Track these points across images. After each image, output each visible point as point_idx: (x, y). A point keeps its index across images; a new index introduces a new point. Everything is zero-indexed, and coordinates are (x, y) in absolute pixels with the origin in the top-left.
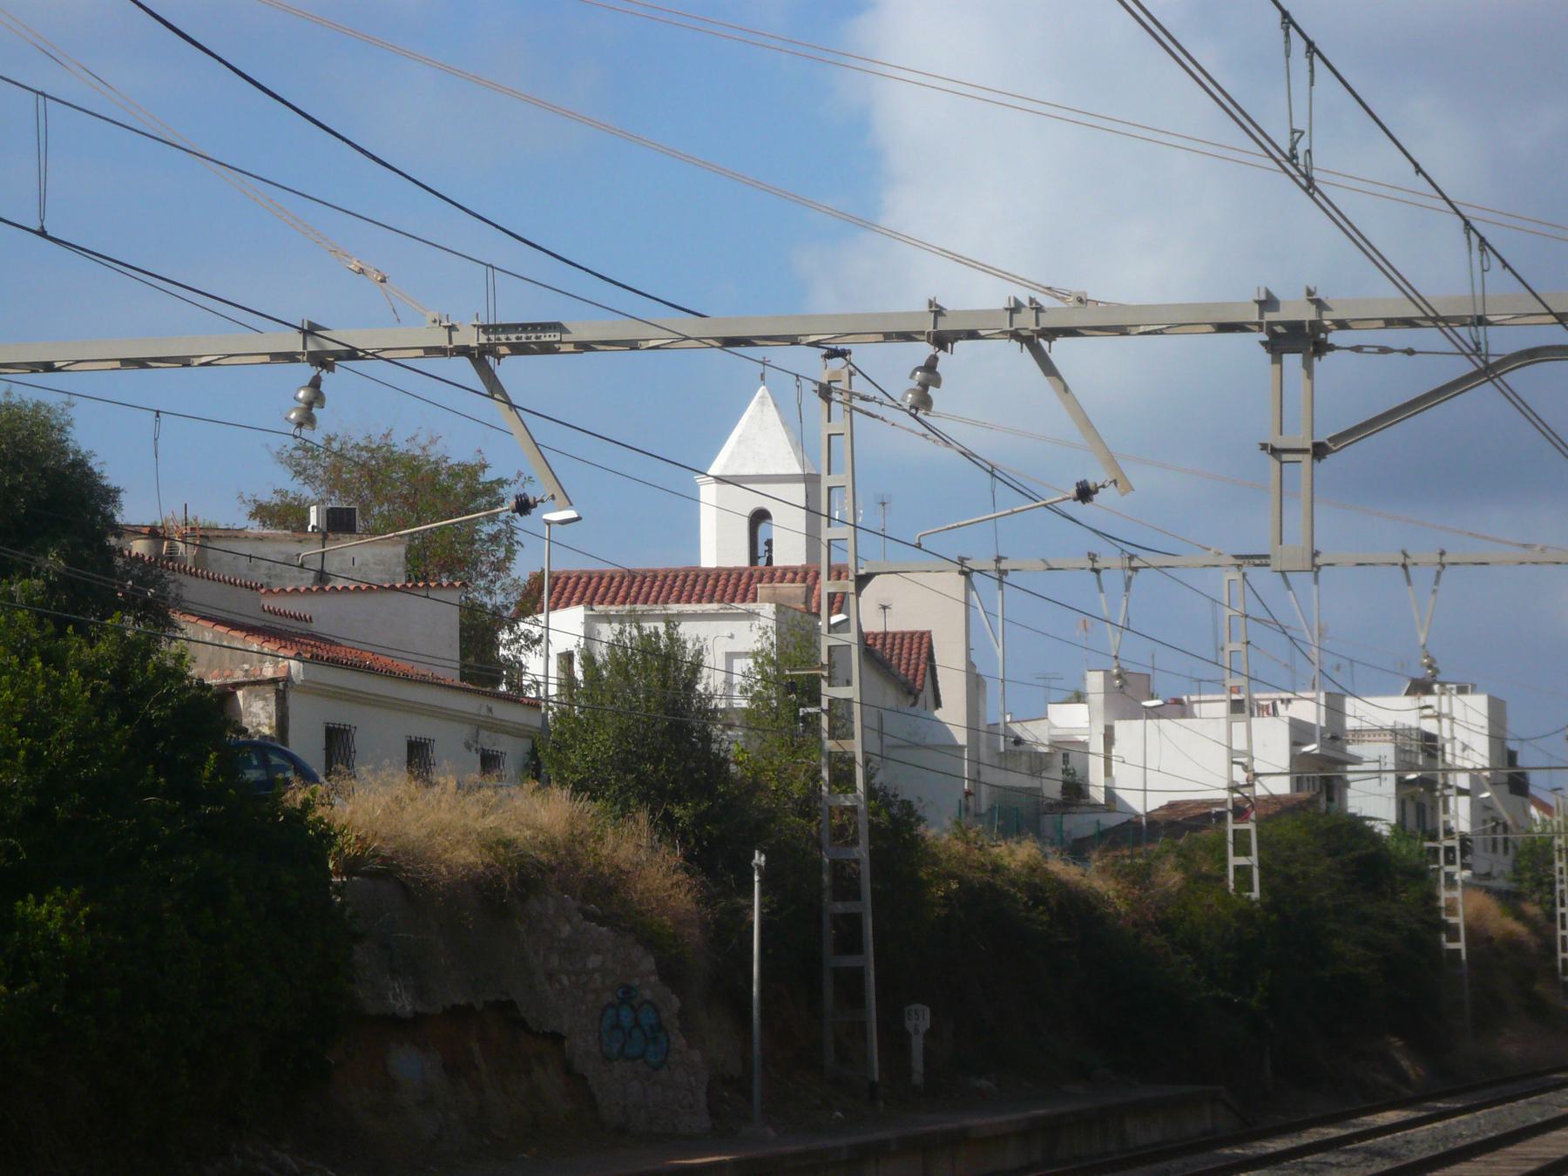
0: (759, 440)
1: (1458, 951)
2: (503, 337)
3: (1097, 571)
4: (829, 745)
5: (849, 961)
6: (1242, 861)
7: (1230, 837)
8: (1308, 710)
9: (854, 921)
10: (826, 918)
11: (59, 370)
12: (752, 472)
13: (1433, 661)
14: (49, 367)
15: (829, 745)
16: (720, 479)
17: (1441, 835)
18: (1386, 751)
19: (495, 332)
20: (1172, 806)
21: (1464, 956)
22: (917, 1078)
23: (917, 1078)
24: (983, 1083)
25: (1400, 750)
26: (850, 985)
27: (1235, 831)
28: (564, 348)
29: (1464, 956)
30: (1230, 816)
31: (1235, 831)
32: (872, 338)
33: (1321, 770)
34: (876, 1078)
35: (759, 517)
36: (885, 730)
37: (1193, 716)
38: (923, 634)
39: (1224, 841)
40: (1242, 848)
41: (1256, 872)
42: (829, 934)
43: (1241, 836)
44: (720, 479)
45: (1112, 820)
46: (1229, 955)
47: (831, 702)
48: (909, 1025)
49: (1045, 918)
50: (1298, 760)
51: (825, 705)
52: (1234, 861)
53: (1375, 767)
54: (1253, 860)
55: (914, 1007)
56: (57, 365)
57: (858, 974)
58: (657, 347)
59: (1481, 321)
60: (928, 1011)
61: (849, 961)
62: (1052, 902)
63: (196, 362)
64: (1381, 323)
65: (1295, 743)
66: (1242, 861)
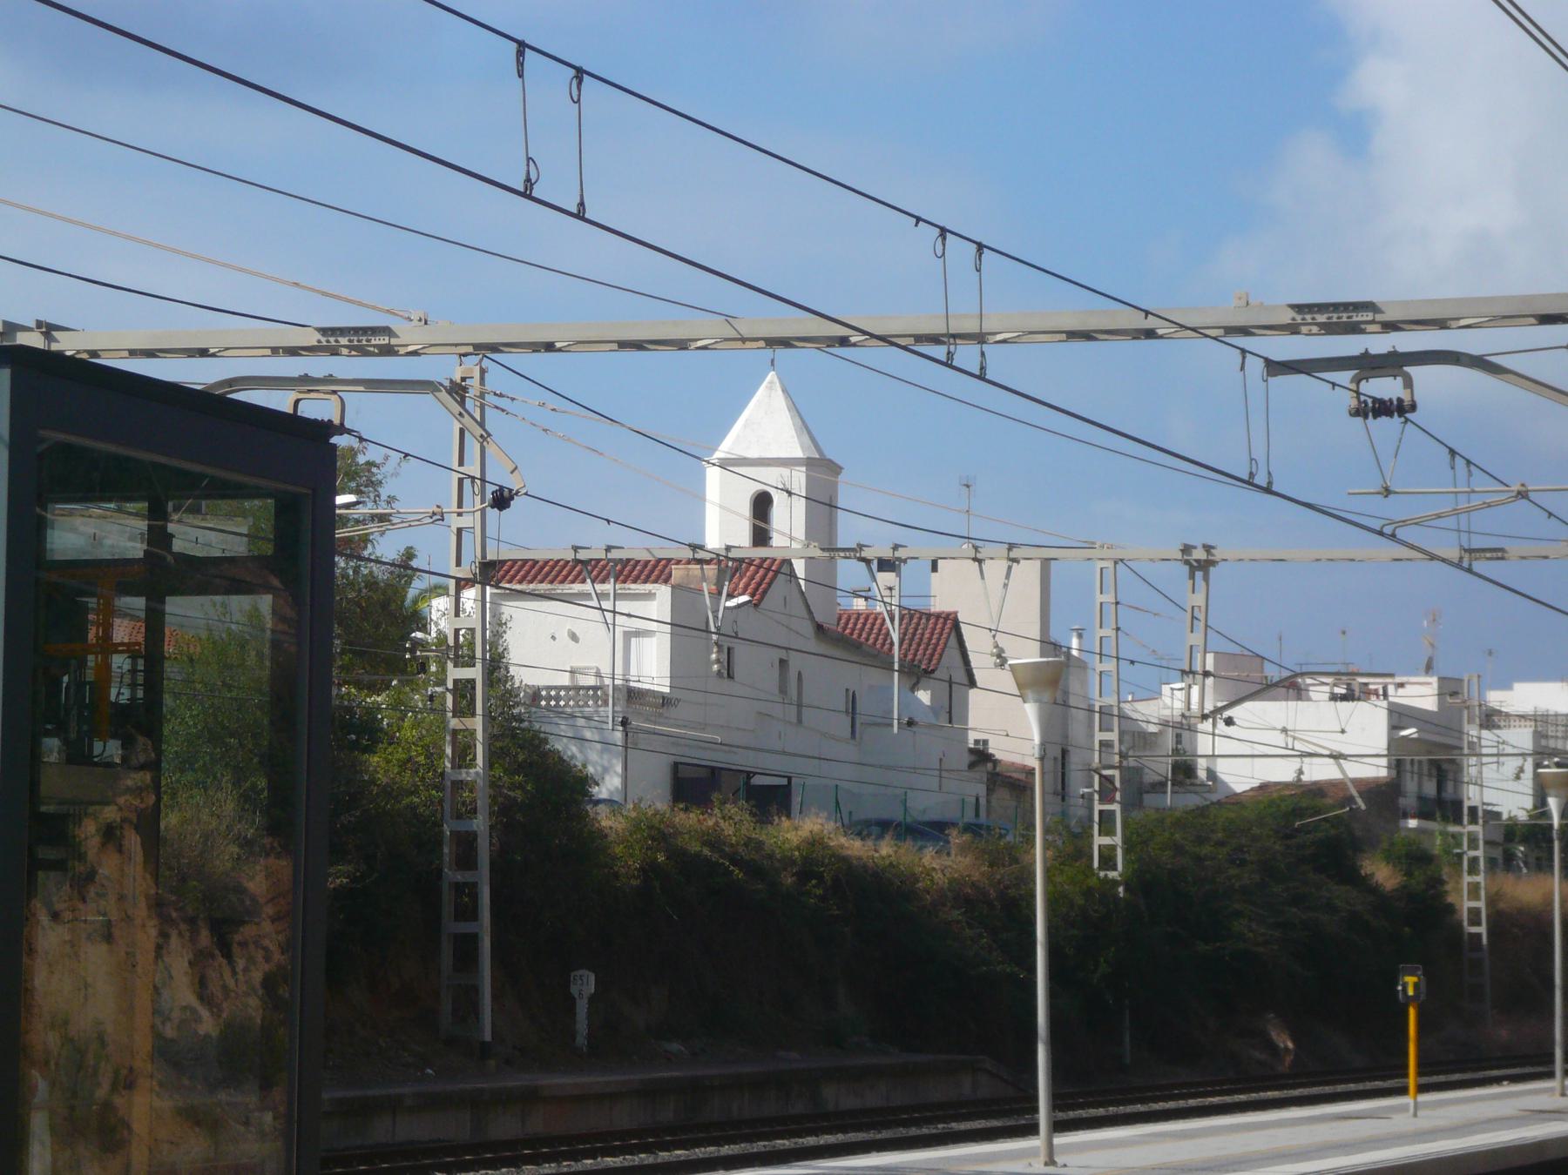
0: (766, 427)
1: (1479, 935)
2: (1308, 317)
3: (980, 561)
4: (454, 723)
5: (464, 927)
6: (1106, 841)
7: (1096, 818)
8: (1422, 695)
9: (472, 890)
10: (445, 886)
11: (214, 355)
12: (756, 455)
13: (1002, 650)
14: (204, 353)
15: (454, 723)
16: (724, 464)
17: (1466, 819)
18: (1521, 737)
19: (1310, 312)
20: (1264, 787)
21: (1485, 940)
22: (581, 1040)
23: (581, 1040)
24: (675, 1047)
25: (1538, 736)
26: (466, 948)
27: (1101, 812)
28: (1370, 328)
29: (1485, 940)
30: (1096, 797)
31: (1101, 812)
32: (1059, 337)
33: (1429, 753)
34: (488, 1037)
35: (762, 504)
36: (805, 701)
37: (1309, 699)
38: (948, 614)
39: (1091, 819)
40: (1107, 830)
41: (1119, 852)
42: (447, 896)
43: (1106, 818)
44: (724, 464)
45: (1214, 798)
46: (1075, 932)
47: (456, 681)
48: (574, 990)
49: (819, 892)
50: (1395, 744)
51: (450, 685)
52: (1099, 840)
53: (1494, 751)
54: (1117, 840)
55: (581, 972)
56: (558, 345)
57: (474, 939)
58: (1004, 341)
59: (980, 338)
60: (592, 978)
61: (464, 927)
62: (827, 877)
63: (402, 351)
64: (126, 354)
65: (1394, 727)
66: (1106, 841)
